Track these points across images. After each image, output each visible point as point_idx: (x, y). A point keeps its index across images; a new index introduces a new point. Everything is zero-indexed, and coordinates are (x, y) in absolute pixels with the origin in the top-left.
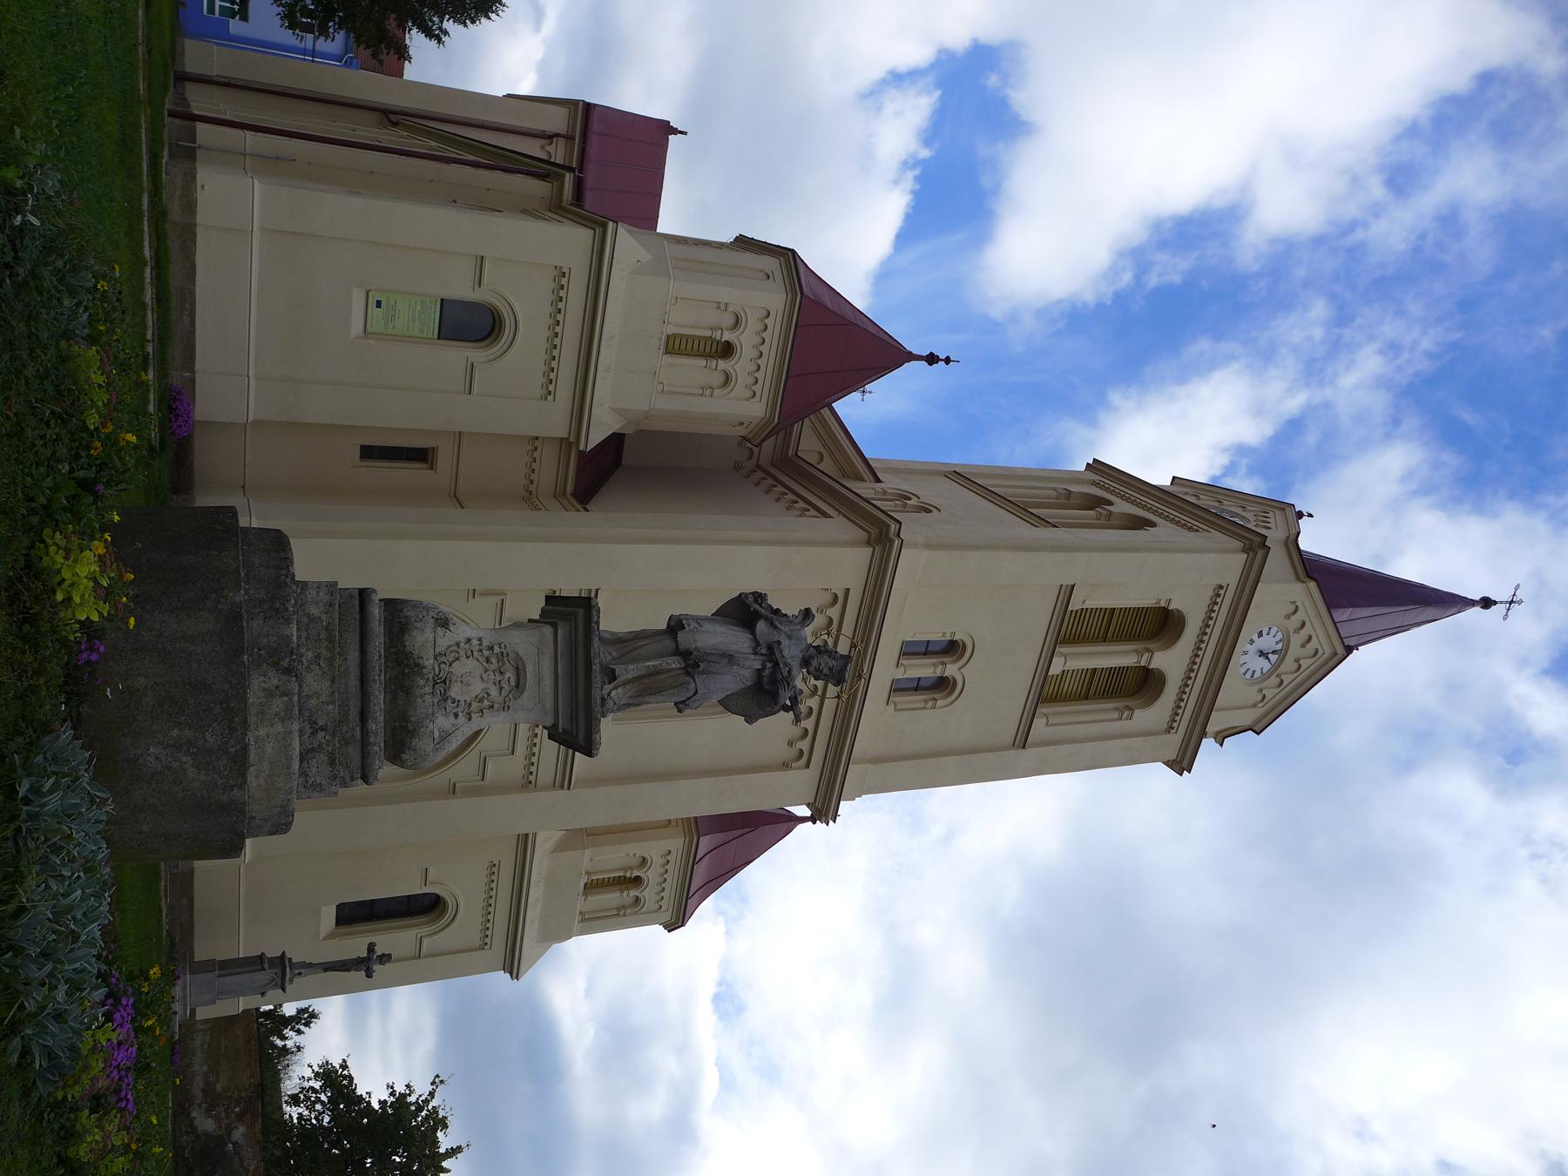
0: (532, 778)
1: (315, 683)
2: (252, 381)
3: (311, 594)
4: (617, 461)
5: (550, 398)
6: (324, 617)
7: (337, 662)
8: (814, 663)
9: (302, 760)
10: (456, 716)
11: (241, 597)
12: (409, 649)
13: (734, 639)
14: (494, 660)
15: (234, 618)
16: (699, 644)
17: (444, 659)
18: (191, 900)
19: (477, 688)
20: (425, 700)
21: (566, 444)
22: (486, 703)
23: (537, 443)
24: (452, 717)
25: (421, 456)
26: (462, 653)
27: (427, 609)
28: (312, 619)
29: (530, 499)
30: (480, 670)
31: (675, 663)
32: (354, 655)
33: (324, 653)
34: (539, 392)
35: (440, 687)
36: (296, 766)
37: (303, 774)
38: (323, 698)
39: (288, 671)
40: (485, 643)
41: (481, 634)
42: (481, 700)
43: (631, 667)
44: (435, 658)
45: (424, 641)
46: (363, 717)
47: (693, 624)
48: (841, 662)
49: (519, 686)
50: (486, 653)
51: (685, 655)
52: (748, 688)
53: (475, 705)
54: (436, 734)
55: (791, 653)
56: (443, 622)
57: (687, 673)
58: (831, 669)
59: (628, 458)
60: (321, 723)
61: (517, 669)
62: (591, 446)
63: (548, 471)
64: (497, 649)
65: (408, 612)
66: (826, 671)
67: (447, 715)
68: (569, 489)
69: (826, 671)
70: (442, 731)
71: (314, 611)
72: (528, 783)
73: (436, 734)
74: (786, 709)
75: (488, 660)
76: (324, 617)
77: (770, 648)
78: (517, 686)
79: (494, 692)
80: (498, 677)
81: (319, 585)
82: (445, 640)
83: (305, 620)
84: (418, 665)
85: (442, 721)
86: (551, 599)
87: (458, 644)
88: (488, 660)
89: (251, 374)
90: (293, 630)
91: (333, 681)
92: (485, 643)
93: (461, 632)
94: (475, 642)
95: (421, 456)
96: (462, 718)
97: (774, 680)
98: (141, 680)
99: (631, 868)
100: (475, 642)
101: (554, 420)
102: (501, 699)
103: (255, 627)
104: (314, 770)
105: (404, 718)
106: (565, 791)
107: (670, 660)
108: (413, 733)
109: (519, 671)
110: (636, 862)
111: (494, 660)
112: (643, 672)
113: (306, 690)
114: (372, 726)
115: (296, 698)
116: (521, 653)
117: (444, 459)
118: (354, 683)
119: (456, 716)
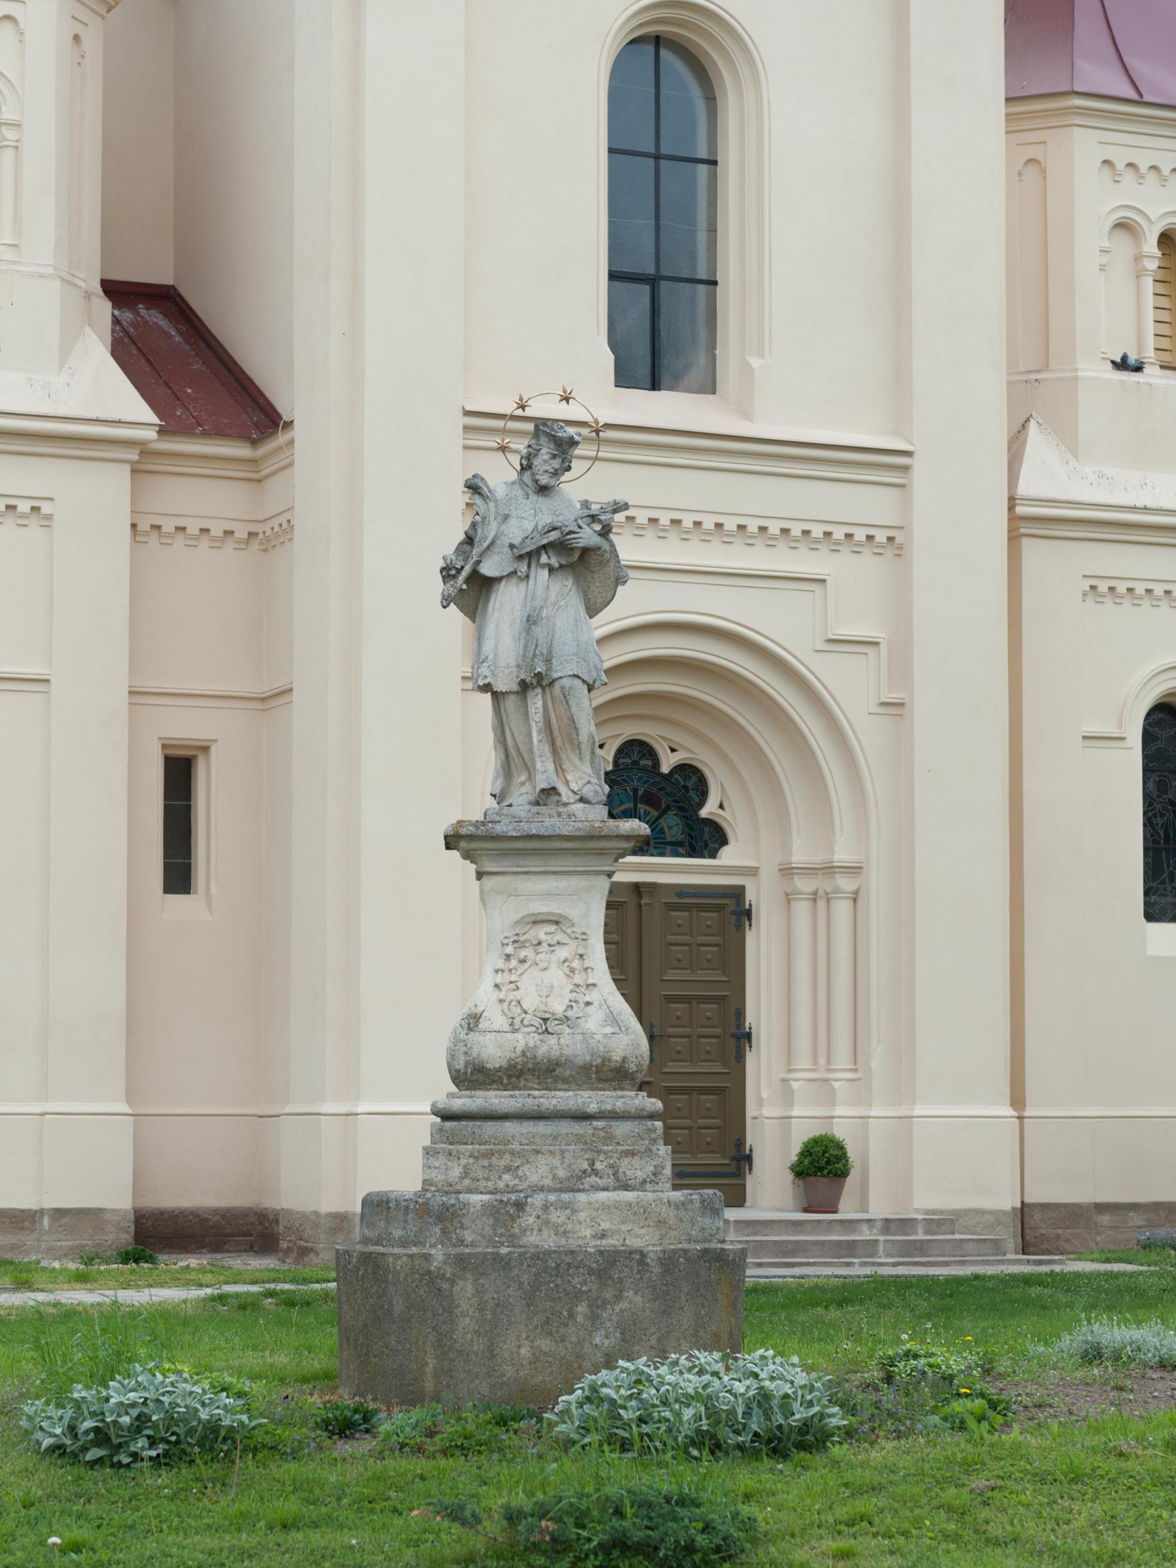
0: (881, 537)
1: (539, 1171)
2: (50, 1107)
3: (438, 1177)
4: (165, 298)
5: (46, 508)
6: (463, 1162)
7: (516, 1146)
8: (544, 480)
9: (626, 1187)
10: (588, 1004)
11: (438, 1254)
12: (504, 1064)
13: (507, 603)
14: (523, 954)
15: (461, 1262)
16: (513, 662)
17: (517, 1021)
18: (1101, 1208)
19: (556, 975)
20: (566, 1045)
21: (144, 464)
22: (576, 964)
23: (144, 526)
24: (590, 1009)
25: (179, 773)
26: (511, 996)
27: (456, 1040)
28: (466, 1174)
29: (267, 538)
30: (534, 971)
31: (536, 702)
32: (510, 1127)
33: (506, 1160)
34: (34, 532)
35: (552, 1026)
36: (630, 1196)
37: (642, 1186)
38: (556, 1161)
39: (520, 1206)
40: (500, 964)
41: (489, 969)
42: (572, 971)
43: (539, 765)
44: (515, 1031)
45: (494, 1049)
46: (582, 1117)
47: (484, 670)
48: (544, 440)
49: (556, 921)
50: (513, 963)
51: (524, 687)
52: (577, 582)
53: (577, 979)
54: (609, 1030)
55: (527, 520)
56: (473, 1021)
57: (551, 684)
58: (554, 457)
59: (156, 271)
60: (585, 1165)
61: (534, 923)
62: (149, 415)
63: (206, 490)
64: (509, 950)
65: (460, 1064)
66: (556, 463)
67: (587, 1016)
68: (242, 450)
69: (556, 463)
70: (605, 1023)
71: (456, 1172)
72: (892, 544)
73: (609, 1030)
74: (605, 532)
75: (523, 961)
76: (463, 1162)
77: (520, 557)
78: (557, 923)
79: (562, 953)
80: (544, 947)
81: (428, 1167)
82: (495, 1019)
83: (466, 1182)
84: (524, 1053)
85: (594, 1022)
86: (447, 848)
87: (501, 1001)
88: (523, 961)
89: (39, 1110)
90: (476, 1199)
91: (537, 1152)
92: (500, 964)
93: (485, 997)
94: (499, 979)
95: (179, 773)
96: (593, 996)
97: (560, 546)
98: (523, 1351)
99: (1138, 258)
100: (499, 979)
101: (94, 496)
102: (573, 944)
103: (475, 1235)
104: (638, 1173)
105: (586, 1069)
106: (916, 463)
107: (532, 710)
108: (606, 1060)
109: (538, 921)
110: (1123, 246)
111: (523, 954)
112: (546, 748)
113: (547, 1182)
114: (593, 1108)
115: (552, 1197)
116: (517, 917)
117: (184, 726)
118: (542, 1128)
119: (588, 1004)
